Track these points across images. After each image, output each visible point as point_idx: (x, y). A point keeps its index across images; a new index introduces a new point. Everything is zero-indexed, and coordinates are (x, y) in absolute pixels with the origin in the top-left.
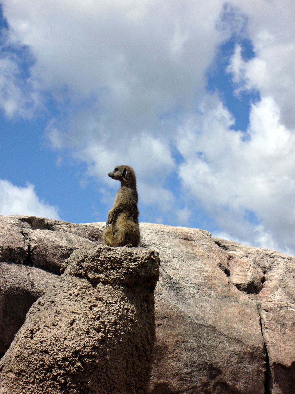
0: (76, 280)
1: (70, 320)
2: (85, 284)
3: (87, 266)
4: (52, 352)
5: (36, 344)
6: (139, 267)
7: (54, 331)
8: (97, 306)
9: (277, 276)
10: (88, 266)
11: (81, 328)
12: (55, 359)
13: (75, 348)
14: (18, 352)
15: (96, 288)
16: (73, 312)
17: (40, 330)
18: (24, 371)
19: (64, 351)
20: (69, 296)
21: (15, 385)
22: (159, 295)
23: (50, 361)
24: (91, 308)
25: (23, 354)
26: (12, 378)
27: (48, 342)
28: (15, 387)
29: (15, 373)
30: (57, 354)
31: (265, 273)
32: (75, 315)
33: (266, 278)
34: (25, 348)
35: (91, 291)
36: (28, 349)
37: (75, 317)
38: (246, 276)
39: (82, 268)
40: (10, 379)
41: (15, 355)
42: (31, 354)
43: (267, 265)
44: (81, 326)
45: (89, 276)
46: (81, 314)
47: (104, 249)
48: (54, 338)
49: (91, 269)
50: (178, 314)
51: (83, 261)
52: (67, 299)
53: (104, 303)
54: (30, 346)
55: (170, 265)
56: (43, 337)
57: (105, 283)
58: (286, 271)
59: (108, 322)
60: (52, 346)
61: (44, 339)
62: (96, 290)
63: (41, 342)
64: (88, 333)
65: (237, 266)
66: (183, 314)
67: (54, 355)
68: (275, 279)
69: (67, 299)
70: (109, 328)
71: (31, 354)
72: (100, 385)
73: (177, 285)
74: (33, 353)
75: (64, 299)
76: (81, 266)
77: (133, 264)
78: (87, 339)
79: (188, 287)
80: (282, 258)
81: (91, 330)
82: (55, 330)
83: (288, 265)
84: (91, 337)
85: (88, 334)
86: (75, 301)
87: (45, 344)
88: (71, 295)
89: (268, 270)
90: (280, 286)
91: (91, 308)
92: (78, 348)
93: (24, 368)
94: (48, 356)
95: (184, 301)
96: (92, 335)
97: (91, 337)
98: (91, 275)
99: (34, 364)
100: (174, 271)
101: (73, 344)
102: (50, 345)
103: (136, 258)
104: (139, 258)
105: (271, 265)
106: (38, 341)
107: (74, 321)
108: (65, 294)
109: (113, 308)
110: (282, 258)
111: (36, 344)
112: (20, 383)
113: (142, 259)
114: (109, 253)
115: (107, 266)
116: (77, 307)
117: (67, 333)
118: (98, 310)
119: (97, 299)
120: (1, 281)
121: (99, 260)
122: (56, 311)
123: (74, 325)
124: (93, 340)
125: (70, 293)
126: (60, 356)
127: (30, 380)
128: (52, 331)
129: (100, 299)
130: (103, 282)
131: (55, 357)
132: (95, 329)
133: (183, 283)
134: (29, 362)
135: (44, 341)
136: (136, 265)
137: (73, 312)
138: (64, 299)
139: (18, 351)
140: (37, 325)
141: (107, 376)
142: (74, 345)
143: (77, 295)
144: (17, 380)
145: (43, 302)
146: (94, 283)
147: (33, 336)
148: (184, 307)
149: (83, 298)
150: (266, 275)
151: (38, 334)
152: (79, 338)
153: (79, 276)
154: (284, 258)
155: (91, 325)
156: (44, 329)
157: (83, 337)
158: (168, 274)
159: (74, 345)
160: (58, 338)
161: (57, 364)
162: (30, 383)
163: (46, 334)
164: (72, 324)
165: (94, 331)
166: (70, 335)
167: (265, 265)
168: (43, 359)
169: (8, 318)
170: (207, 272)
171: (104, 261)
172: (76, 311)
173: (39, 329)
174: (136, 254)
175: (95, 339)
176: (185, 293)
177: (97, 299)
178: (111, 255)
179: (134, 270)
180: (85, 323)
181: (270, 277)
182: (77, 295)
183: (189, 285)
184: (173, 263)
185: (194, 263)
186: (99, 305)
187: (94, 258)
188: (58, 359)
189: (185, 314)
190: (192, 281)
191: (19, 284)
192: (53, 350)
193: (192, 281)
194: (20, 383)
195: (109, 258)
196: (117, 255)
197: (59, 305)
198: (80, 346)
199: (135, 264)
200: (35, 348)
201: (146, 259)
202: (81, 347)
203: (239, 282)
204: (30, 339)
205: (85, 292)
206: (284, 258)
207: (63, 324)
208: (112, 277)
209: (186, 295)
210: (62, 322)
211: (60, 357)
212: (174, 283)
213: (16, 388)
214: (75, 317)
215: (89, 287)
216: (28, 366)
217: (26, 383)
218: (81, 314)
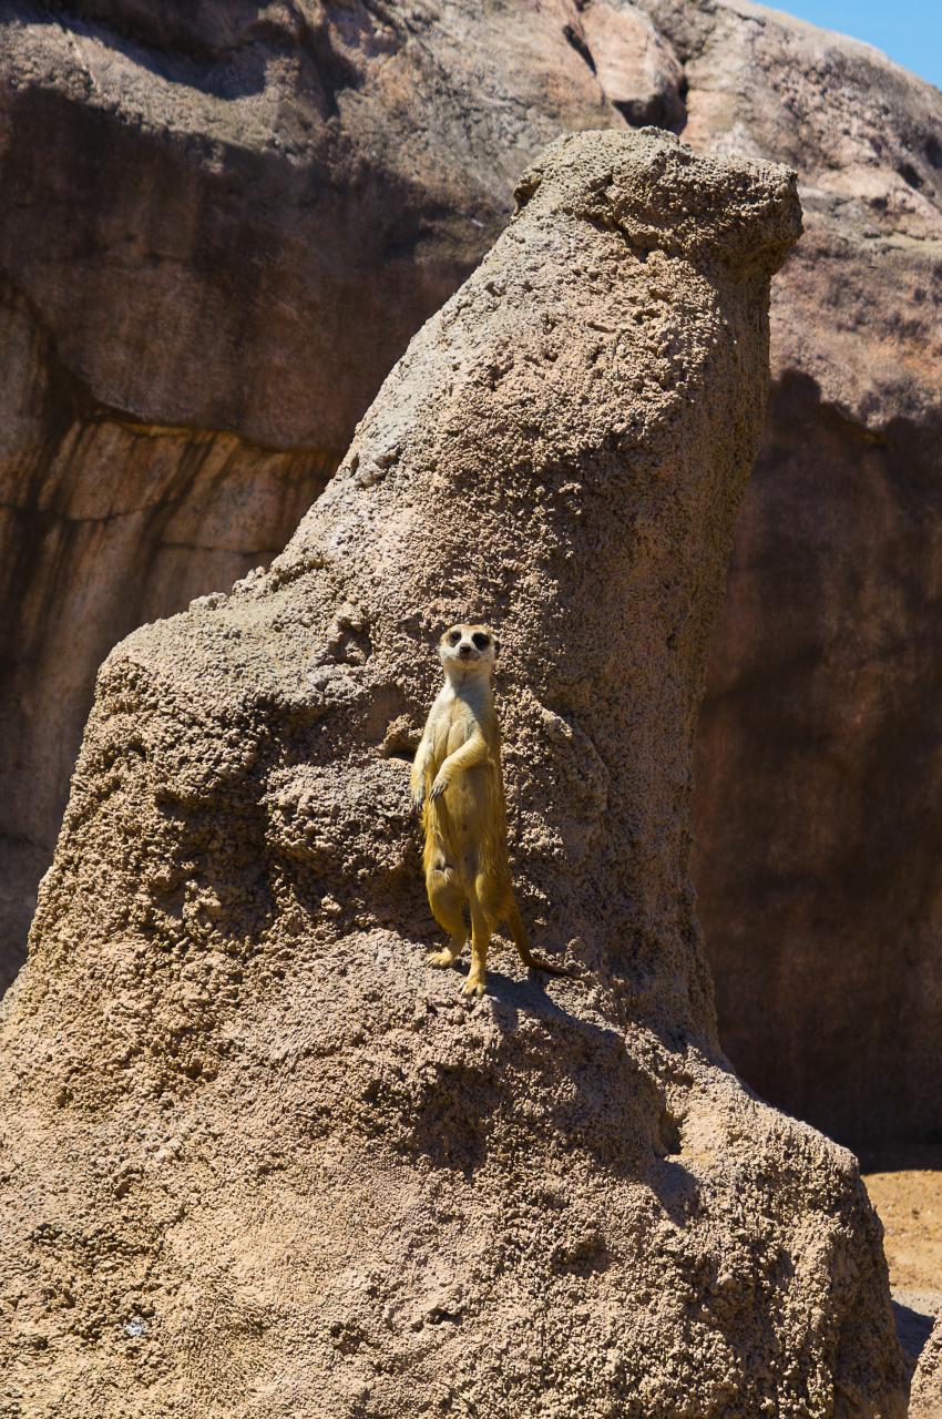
0: (584, 230)
1: (589, 346)
2: (615, 246)
3: (622, 197)
4: (551, 433)
5: (507, 407)
6: (761, 217)
7: (553, 375)
8: (659, 316)
9: (725, 81)
10: (626, 199)
11: (622, 373)
12: (561, 452)
13: (612, 425)
14: (455, 422)
15: (646, 262)
16: (592, 325)
17: (517, 369)
18: (476, 474)
19: (583, 432)
20: (573, 277)
21: (447, 507)
22: (419, 132)
23: (547, 456)
24: (639, 319)
25: (471, 429)
26: (437, 489)
27: (541, 405)
28: (448, 513)
29: (448, 476)
30: (565, 438)
31: (683, 60)
32: (603, 334)
33: (691, 82)
34: (476, 413)
35: (632, 270)
36: (484, 417)
37: (601, 339)
38: (641, 73)
39: (604, 199)
40: (432, 490)
41: (447, 427)
42: (494, 432)
43: (693, 35)
44: (618, 365)
45: (627, 226)
46: (614, 331)
47: (672, 156)
48: (555, 395)
49: (627, 207)
50: (475, 198)
51: (609, 181)
52: (568, 283)
53: (676, 309)
54: (491, 410)
55: (440, 31)
56: (526, 389)
57: (672, 251)
58: (754, 63)
59: (690, 363)
60: (552, 414)
61: (530, 395)
62: (644, 267)
63: (523, 404)
64: (639, 388)
65: (607, 35)
66: (488, 201)
67: (558, 440)
68: (722, 90)
69: (568, 283)
70: (691, 378)
71: (494, 432)
72: (658, 525)
73: (465, 103)
74: (501, 430)
75: (560, 282)
76: (602, 194)
77: (748, 206)
78: (638, 405)
79: (495, 108)
80: (740, 16)
81: (646, 381)
82: (555, 370)
83: (758, 46)
84: (648, 399)
85: (640, 391)
86: (592, 292)
87: (534, 410)
88: (577, 273)
89: (696, 54)
90: (737, 114)
91: (639, 319)
92: (619, 427)
93: (474, 466)
94: (540, 442)
95: (489, 158)
96: (650, 394)
97: (648, 399)
98: (633, 226)
99: (502, 459)
100: (452, 52)
101: (604, 414)
102: (547, 412)
103: (757, 190)
104: (766, 190)
105: (704, 37)
106: (514, 399)
107: (598, 351)
108: (562, 268)
109: (698, 323)
110: (740, 16)
111: (507, 407)
112: (463, 502)
113: (771, 196)
114: (685, 169)
115: (681, 207)
116: (598, 309)
117: (587, 382)
118: (664, 329)
119: (654, 295)
120: (3, 66)
121: (660, 188)
122: (547, 316)
123: (601, 363)
124: (654, 407)
125: (574, 267)
126: (575, 443)
127: (489, 500)
128: (548, 374)
129: (665, 298)
130: (665, 249)
131: (561, 446)
132: (656, 379)
133: (480, 95)
134: (487, 450)
135: (529, 399)
136: (757, 209)
137: (592, 325)
138: (560, 282)
139: (458, 418)
140: (506, 354)
141: (677, 502)
142: (608, 419)
143: (594, 277)
144: (452, 495)
145: (501, 285)
146: (641, 247)
147: (496, 383)
148: (491, 177)
149: (612, 285)
150: (688, 70)
151: (510, 379)
152: (619, 400)
153: (596, 221)
154: (746, 19)
155: (647, 367)
156: (527, 366)
157: (628, 398)
158: (436, 59)
159: (608, 419)
160: (566, 395)
161: (566, 465)
162: (489, 507)
163: (531, 381)
164: (594, 358)
165: (655, 385)
166: (595, 389)
167: (685, 37)
168: (528, 447)
169: (17, 186)
170: (540, 59)
171: (672, 190)
172: (598, 323)
173: (511, 367)
174: (757, 180)
175: (659, 405)
176: (490, 131)
177: (654, 295)
178: (692, 177)
179: (750, 222)
180: (628, 358)
181: (705, 79)
182: (594, 277)
183: (499, 103)
184: (448, 23)
185: (502, 23)
186: (664, 314)
187: (648, 178)
188: (570, 452)
189: (494, 199)
190: (506, 91)
191: (51, 78)
192: (555, 426)
193: (506, 91)
194: (463, 502)
195: (685, 184)
196: (708, 176)
197: (547, 299)
198: (622, 421)
199: (754, 206)
200: (506, 417)
201: (779, 196)
202: (624, 425)
203: (626, 96)
204: (488, 390)
205: (615, 271)
206: (746, 19)
207: (573, 356)
208: (692, 236)
209: (495, 136)
210: (568, 351)
211: (574, 445)
212: (456, 93)
213: (451, 516)
214: (601, 339)
215: (624, 257)
216: (487, 461)
217: (478, 505)
218: (614, 331)
